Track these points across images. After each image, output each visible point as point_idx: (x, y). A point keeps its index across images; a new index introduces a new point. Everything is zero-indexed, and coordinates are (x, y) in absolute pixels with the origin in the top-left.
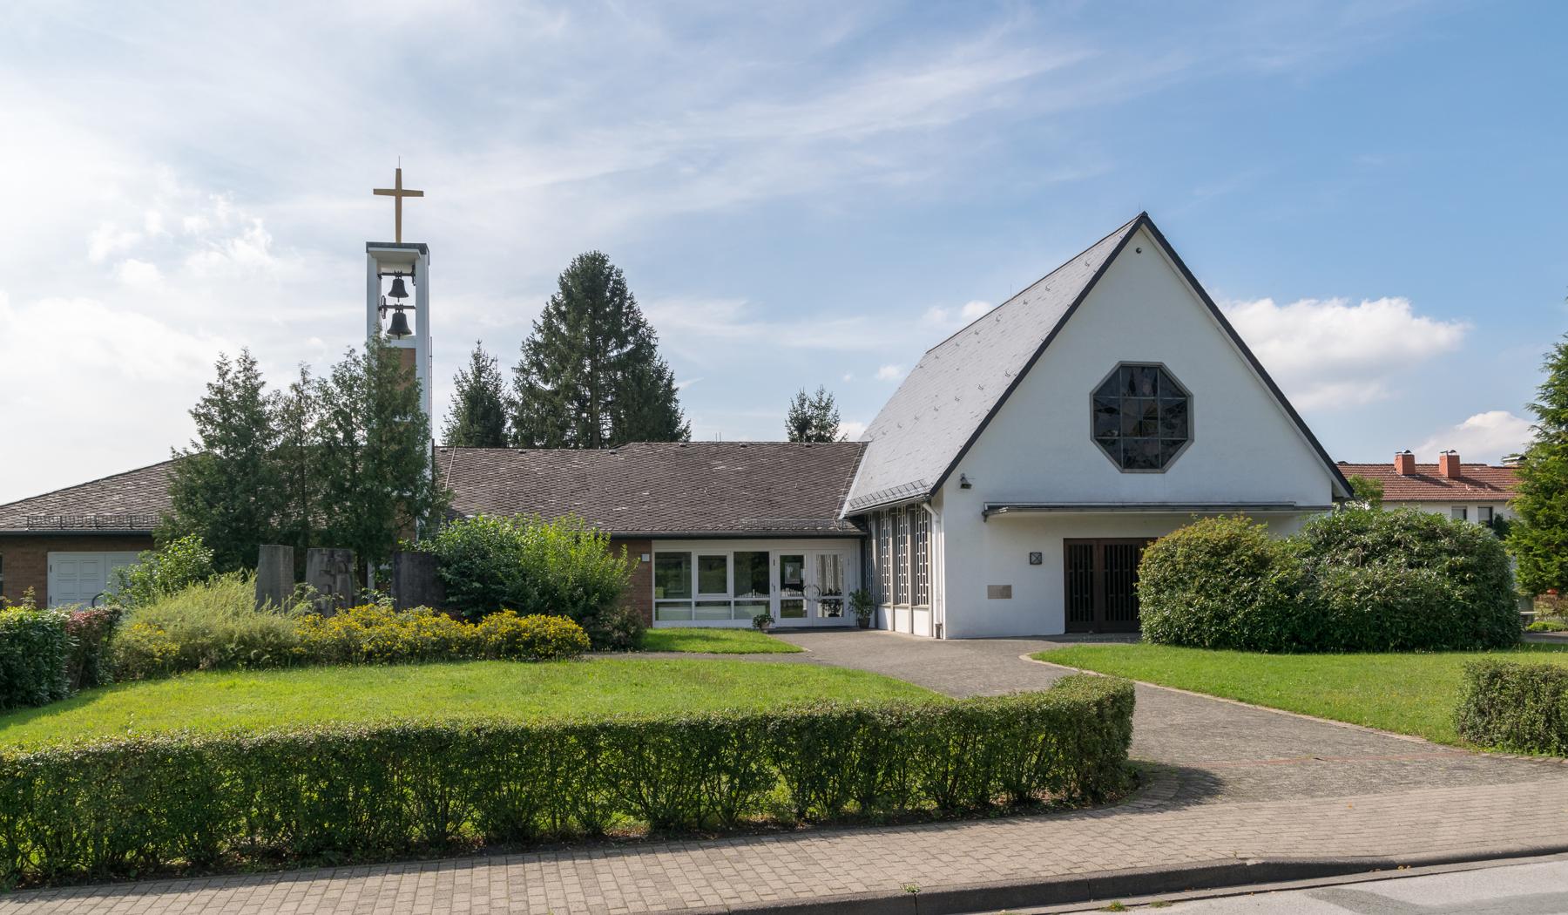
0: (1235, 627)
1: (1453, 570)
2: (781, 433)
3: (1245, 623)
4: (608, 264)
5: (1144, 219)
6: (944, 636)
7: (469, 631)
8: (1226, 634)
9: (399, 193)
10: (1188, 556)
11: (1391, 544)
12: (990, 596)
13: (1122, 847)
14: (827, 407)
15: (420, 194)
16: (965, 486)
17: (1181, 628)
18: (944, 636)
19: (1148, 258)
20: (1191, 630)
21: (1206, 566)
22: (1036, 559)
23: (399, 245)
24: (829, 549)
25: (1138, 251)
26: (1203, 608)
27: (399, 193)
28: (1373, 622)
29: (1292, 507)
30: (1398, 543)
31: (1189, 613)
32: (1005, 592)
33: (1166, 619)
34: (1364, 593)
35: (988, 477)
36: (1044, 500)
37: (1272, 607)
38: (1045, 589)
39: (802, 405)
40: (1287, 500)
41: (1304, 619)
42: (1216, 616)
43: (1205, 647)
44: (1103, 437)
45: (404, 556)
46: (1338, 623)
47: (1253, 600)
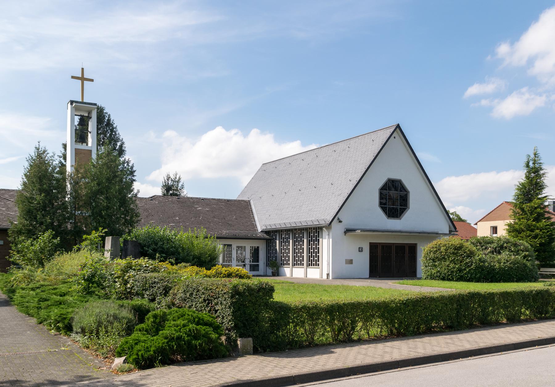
0: (465, 274)
1: (525, 257)
2: (158, 191)
3: (469, 273)
4: (105, 112)
5: (398, 126)
6: (331, 278)
7: (209, 272)
8: (462, 276)
9: (83, 79)
10: (446, 250)
11: (502, 247)
12: (346, 263)
13: (216, 376)
14: (178, 182)
15: (92, 80)
16: (340, 222)
17: (445, 274)
18: (331, 278)
19: (397, 141)
20: (449, 275)
21: (453, 253)
22: (361, 250)
23: (82, 103)
24: (255, 244)
25: (395, 138)
26: (454, 268)
27: (83, 79)
28: (507, 273)
29: (437, 234)
30: (506, 248)
31: (448, 269)
32: (350, 262)
33: (439, 272)
34: (504, 263)
35: (348, 220)
36: (368, 228)
37: (477, 268)
38: (363, 260)
39: (168, 180)
40: (436, 231)
41: (488, 271)
42: (459, 270)
43: (454, 281)
44: (383, 205)
45: (129, 243)
46: (498, 273)
47: (472, 265)
